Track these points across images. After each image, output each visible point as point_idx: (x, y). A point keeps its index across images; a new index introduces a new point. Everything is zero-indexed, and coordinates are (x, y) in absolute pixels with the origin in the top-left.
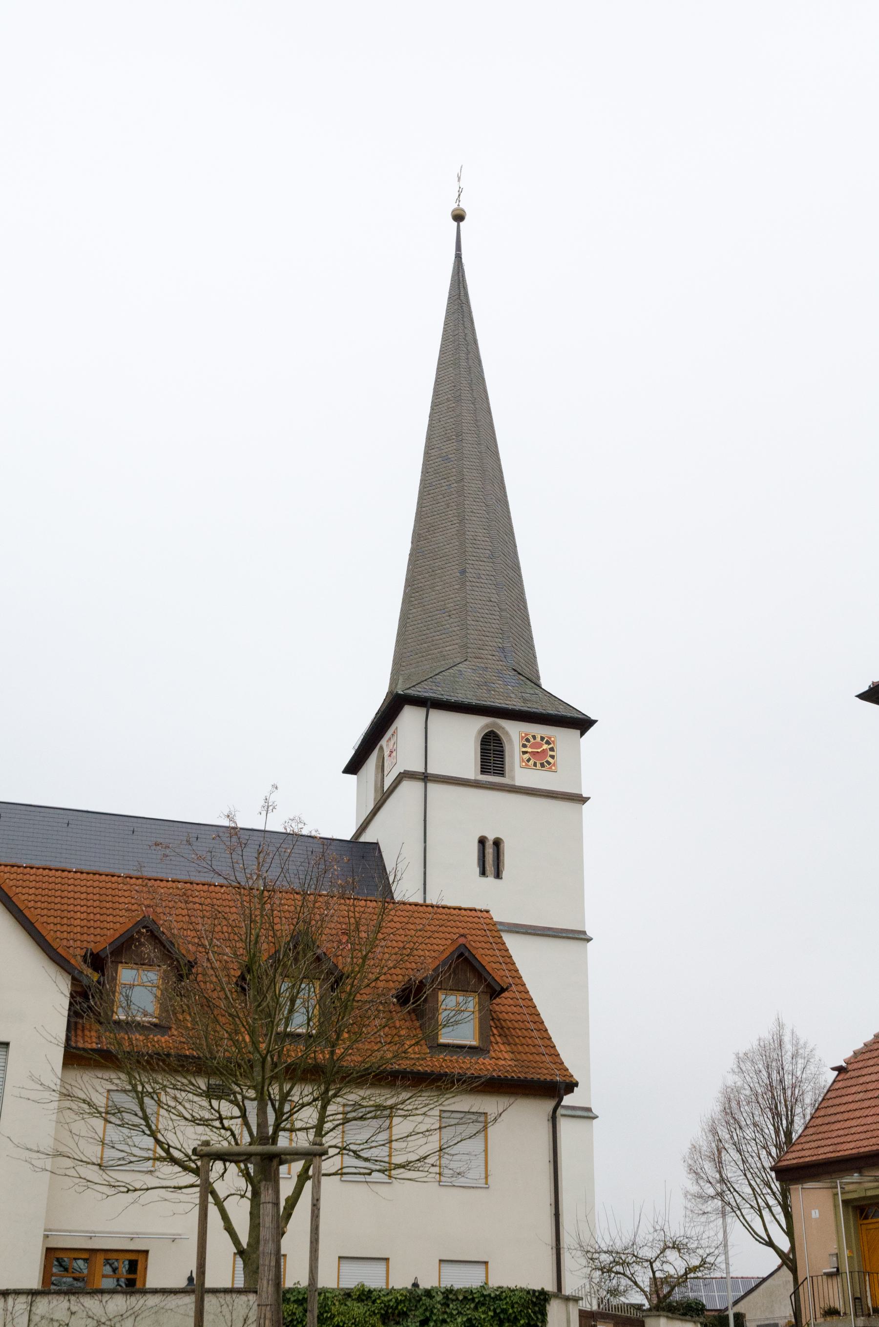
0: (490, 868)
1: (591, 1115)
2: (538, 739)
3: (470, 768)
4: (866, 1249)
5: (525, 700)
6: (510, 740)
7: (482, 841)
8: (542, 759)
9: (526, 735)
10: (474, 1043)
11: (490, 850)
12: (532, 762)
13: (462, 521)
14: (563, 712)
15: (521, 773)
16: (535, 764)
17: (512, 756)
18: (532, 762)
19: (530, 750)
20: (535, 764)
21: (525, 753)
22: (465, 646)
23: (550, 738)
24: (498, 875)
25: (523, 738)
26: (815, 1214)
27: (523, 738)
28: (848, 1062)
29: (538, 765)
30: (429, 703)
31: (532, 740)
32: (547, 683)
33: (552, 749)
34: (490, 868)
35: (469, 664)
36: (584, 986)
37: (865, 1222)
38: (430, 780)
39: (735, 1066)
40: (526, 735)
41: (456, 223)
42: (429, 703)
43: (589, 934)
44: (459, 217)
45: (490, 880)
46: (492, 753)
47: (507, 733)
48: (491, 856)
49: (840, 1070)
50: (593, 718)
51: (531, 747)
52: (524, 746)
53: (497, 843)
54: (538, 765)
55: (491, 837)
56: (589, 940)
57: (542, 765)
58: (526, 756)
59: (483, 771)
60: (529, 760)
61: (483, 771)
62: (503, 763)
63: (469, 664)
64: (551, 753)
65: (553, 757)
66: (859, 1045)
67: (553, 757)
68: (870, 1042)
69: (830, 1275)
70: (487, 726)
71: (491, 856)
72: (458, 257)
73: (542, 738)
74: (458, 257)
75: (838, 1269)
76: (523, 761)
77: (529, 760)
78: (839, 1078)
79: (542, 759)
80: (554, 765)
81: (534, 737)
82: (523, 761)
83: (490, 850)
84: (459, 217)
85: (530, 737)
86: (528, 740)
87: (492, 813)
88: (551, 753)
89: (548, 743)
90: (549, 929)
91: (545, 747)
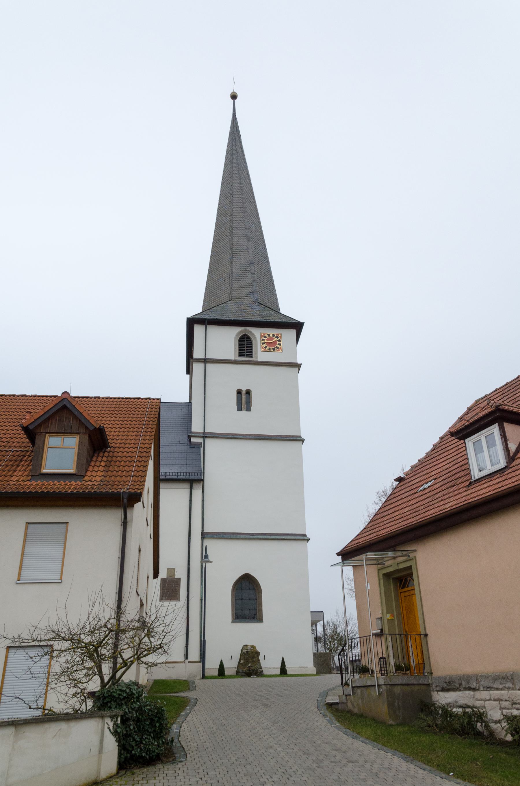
0: (244, 406)
1: (305, 538)
2: (271, 336)
3: (232, 353)
4: (405, 612)
5: (263, 316)
6: (255, 338)
7: (239, 392)
8: (273, 345)
9: (264, 334)
10: (72, 471)
11: (244, 396)
12: (268, 348)
13: (232, 233)
14: (284, 320)
15: (261, 354)
16: (270, 349)
17: (256, 346)
18: (268, 348)
19: (266, 341)
20: (270, 349)
21: (263, 343)
22: (231, 293)
23: (278, 335)
24: (249, 409)
25: (262, 336)
26: (368, 586)
27: (262, 336)
28: (407, 474)
29: (271, 349)
30: (206, 322)
31: (268, 337)
32: (282, 311)
33: (279, 341)
34: (244, 406)
35: (242, 306)
36: (300, 466)
37: (406, 589)
38: (208, 362)
39: (378, 499)
40: (264, 334)
41: (232, 101)
42: (206, 322)
43: (303, 437)
44: (234, 97)
45: (244, 412)
46: (245, 346)
47: (253, 334)
48: (244, 399)
49: (400, 480)
50: (302, 321)
51: (267, 340)
52: (263, 340)
53: (248, 392)
54: (271, 349)
55: (244, 389)
56: (303, 441)
57: (274, 349)
58: (264, 345)
59: (240, 356)
60: (266, 347)
61: (240, 356)
62: (252, 350)
63: (242, 306)
64: (279, 343)
65: (280, 344)
66: (415, 462)
67: (280, 344)
68: (423, 458)
69: (376, 635)
70: (241, 332)
71: (244, 399)
72: (234, 115)
73: (274, 335)
74: (234, 115)
75: (382, 630)
76: (262, 348)
77: (266, 347)
78: (399, 485)
79: (273, 345)
80: (281, 349)
81: (269, 335)
82: (262, 348)
83: (244, 396)
84: (234, 97)
85: (266, 335)
86: (265, 337)
87: (245, 376)
88: (279, 343)
89: (277, 337)
90: (279, 436)
91: (275, 339)
